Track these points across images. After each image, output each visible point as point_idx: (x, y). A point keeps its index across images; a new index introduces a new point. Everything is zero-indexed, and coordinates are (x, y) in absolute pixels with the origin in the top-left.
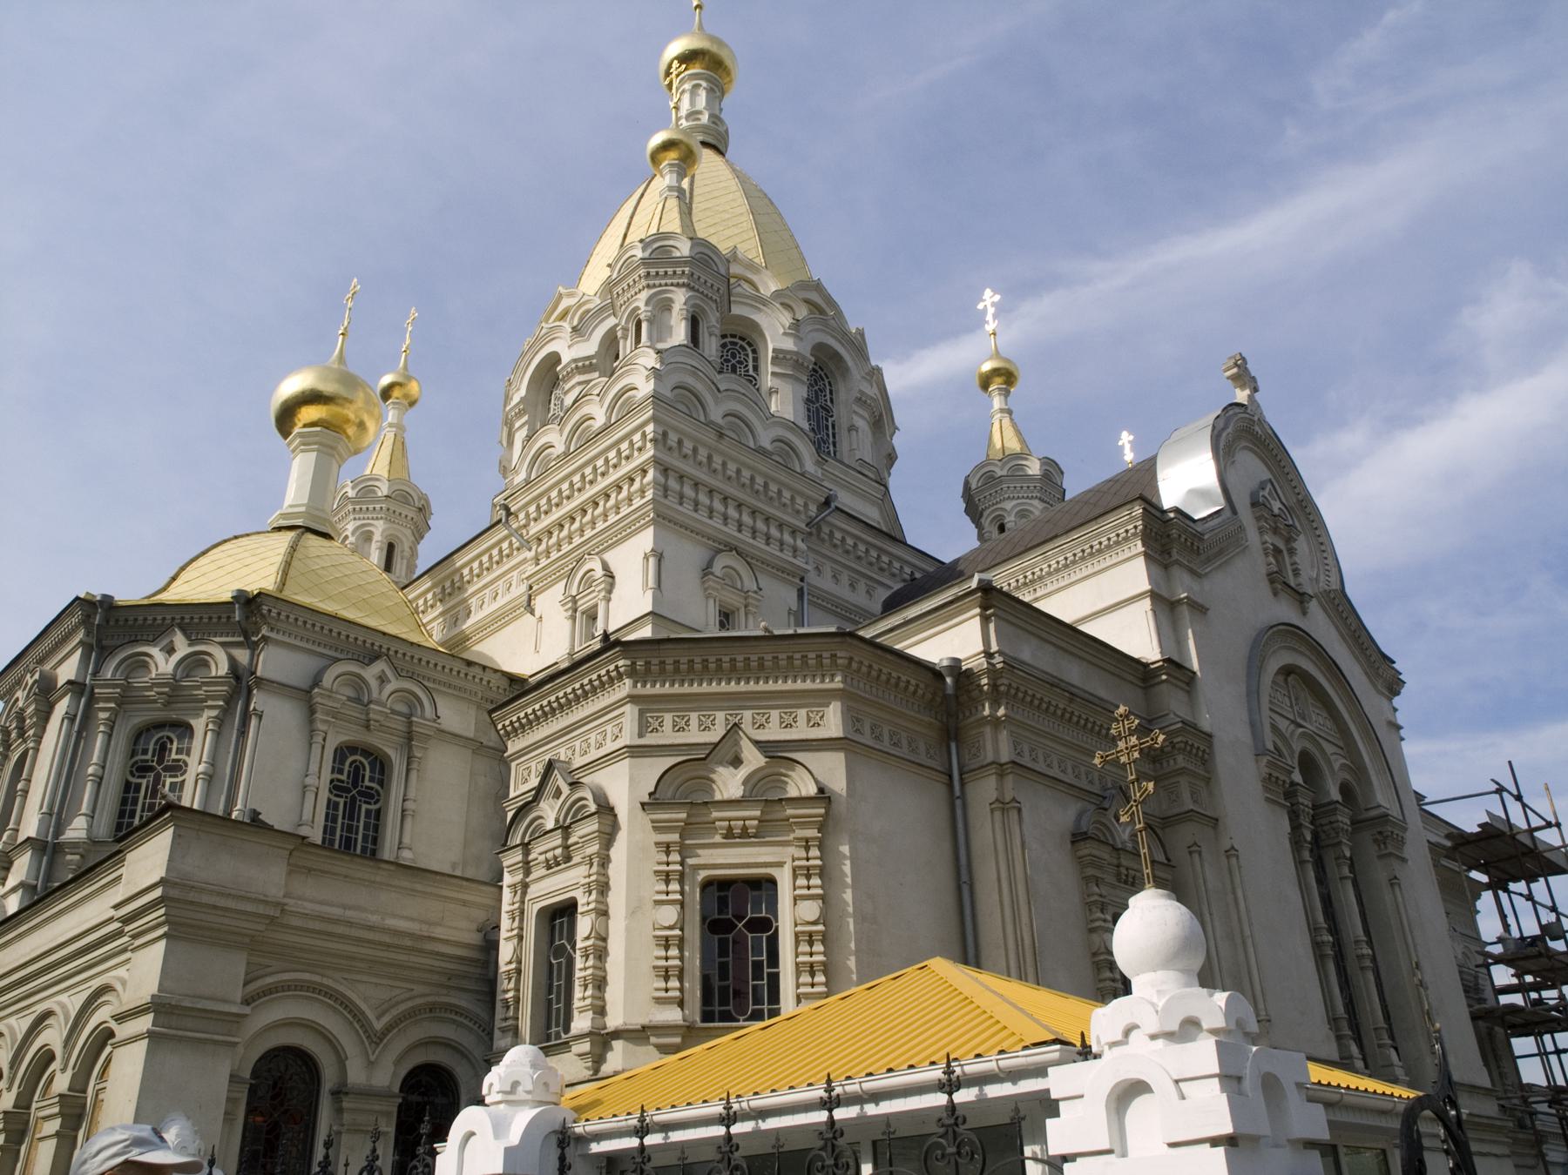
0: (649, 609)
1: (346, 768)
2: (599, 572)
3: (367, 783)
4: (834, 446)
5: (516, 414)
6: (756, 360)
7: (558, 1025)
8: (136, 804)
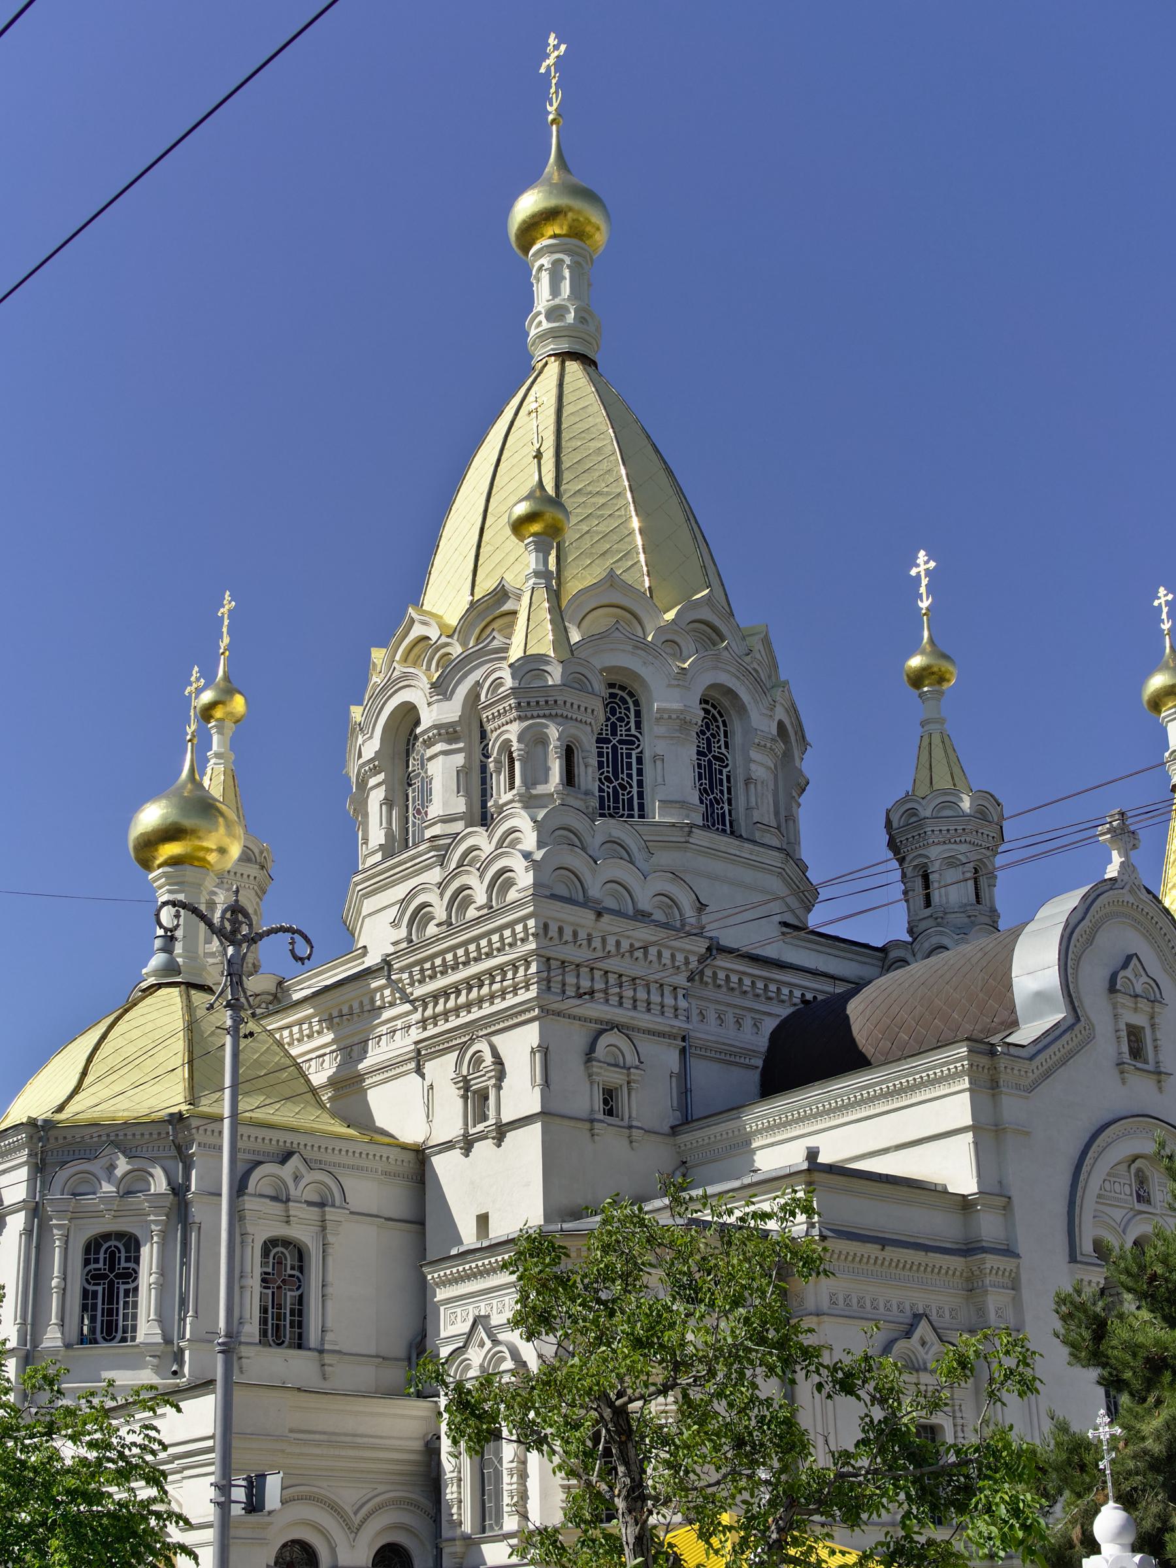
0: (538, 1109)
1: (102, 1256)
2: (488, 1059)
3: (123, 1264)
4: (730, 804)
5: (370, 769)
6: (638, 714)
7: (490, 1520)
8: (96, 1310)
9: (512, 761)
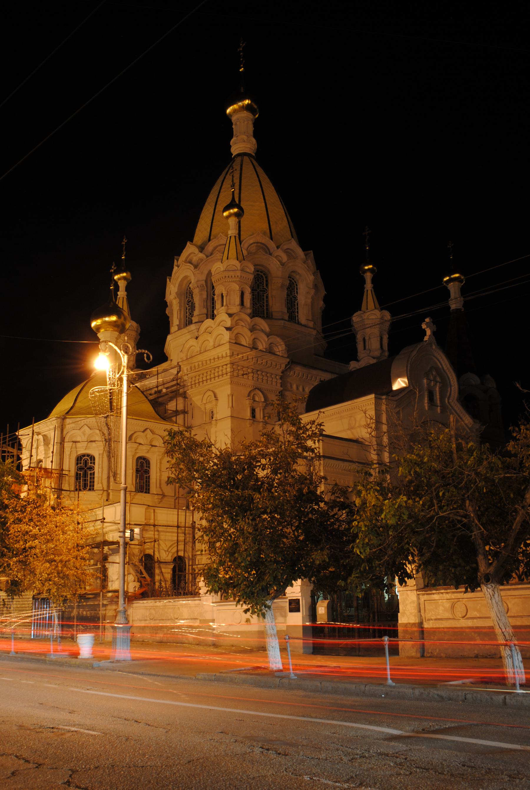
1: (82, 462)
3: (89, 465)
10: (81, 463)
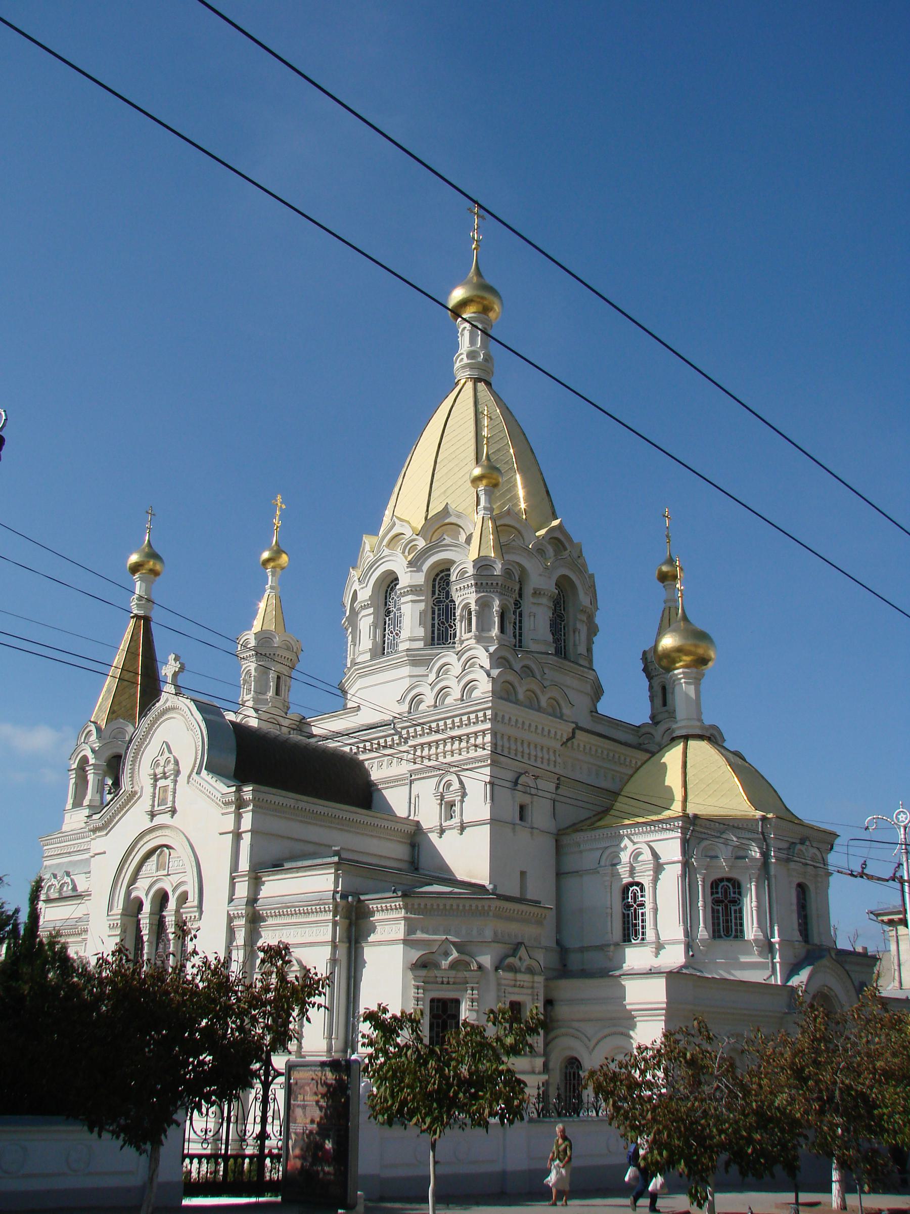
1: (720, 890)
3: (732, 895)
9: (470, 613)
10: (717, 893)
